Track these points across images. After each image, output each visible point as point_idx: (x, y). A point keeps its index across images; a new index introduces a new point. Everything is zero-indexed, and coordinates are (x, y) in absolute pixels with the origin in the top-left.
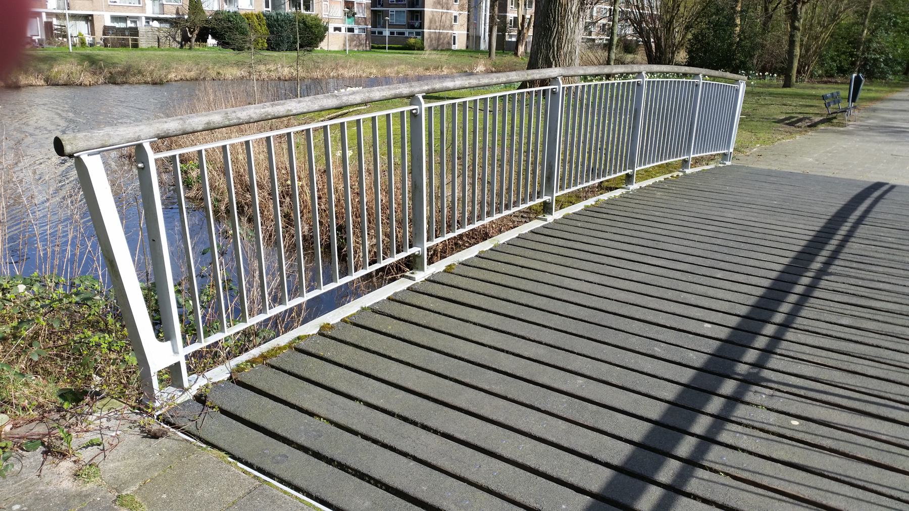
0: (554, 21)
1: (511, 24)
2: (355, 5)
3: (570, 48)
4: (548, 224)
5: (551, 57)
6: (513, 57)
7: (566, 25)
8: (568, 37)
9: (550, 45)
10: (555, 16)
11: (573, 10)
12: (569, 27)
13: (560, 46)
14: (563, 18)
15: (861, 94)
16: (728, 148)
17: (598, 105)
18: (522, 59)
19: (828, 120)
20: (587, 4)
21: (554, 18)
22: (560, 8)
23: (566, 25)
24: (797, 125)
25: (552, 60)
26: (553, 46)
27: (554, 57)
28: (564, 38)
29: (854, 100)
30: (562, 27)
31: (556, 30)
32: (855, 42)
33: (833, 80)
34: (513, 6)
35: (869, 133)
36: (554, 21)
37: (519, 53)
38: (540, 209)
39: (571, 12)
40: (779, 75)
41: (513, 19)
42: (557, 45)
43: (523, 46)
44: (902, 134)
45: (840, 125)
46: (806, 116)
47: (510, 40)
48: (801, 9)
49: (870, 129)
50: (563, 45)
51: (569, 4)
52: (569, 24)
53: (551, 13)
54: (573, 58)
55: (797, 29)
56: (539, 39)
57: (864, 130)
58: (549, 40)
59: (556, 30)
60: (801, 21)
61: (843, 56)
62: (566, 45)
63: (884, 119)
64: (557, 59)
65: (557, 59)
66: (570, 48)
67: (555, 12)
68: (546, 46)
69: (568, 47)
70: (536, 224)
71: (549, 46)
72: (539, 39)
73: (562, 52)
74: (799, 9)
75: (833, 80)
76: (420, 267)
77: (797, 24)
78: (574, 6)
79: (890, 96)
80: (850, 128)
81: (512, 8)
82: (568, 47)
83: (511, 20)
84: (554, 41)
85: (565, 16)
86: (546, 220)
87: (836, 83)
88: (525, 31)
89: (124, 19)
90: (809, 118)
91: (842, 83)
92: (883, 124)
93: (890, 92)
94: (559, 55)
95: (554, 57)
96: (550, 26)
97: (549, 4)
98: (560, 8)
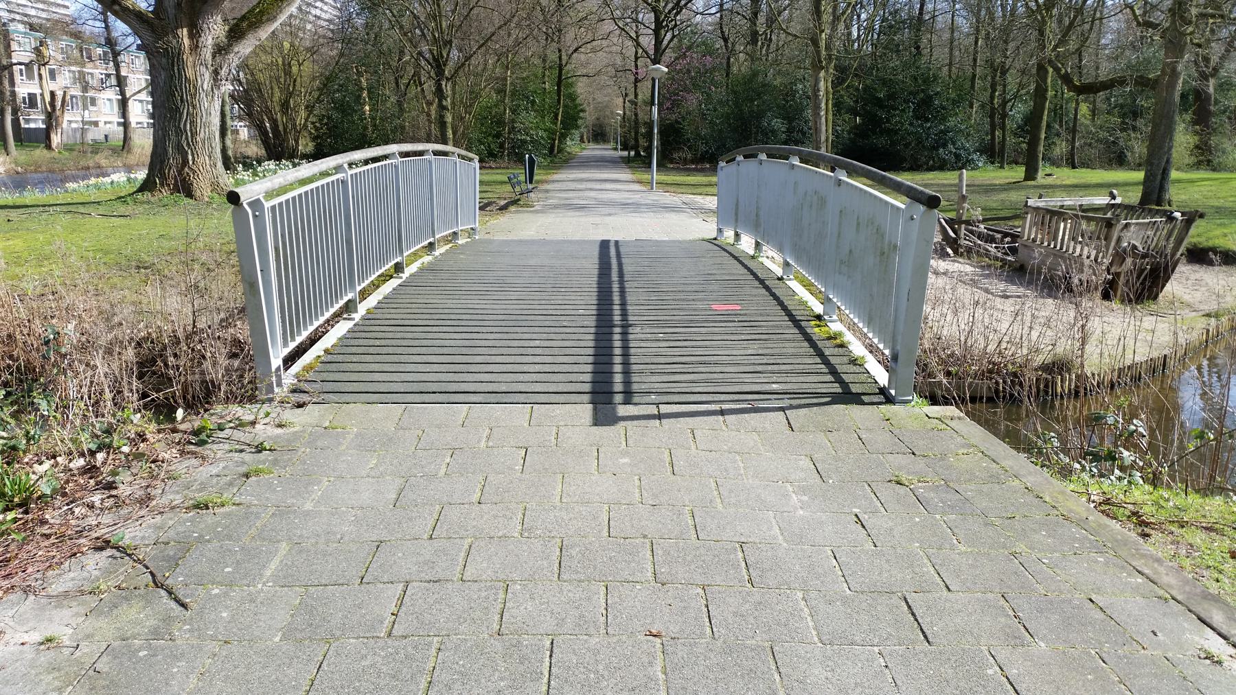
0: (182, 101)
1: (25, 103)
2: (826, 125)
3: (207, 133)
4: (404, 282)
5: (185, 145)
6: (45, 151)
7: (198, 105)
8: (204, 120)
9: (181, 130)
10: (183, 94)
11: (205, 87)
12: (202, 108)
13: (194, 131)
14: (194, 96)
15: (535, 178)
16: (475, 224)
17: (870, 171)
18: (60, 153)
19: (515, 202)
20: (221, 80)
21: (182, 97)
22: (187, 85)
23: (198, 105)
24: (488, 209)
25: (186, 148)
26: (186, 131)
27: (188, 144)
28: (199, 121)
29: (531, 182)
30: (194, 107)
31: (185, 111)
32: (500, 122)
33: (487, 165)
34: (24, 78)
35: (555, 211)
36: (182, 101)
37: (54, 145)
38: (393, 270)
39: (203, 90)
40: (981, 155)
41: (26, 96)
42: (191, 130)
43: (59, 135)
44: (586, 209)
45: (528, 206)
46: (490, 200)
47: (27, 126)
48: (446, 86)
49: (556, 207)
50: (198, 130)
51: (199, 80)
52: (202, 104)
53: (177, 90)
54: (213, 145)
55: (444, 108)
56: (164, 123)
57: (551, 208)
58: (179, 124)
59: (185, 111)
60: (449, 99)
61: (490, 139)
62: (203, 129)
63: (560, 198)
64: (193, 147)
65: (193, 147)
66: (207, 133)
67: (181, 89)
68: (176, 132)
69: (205, 132)
70: (393, 283)
71: (180, 132)
72: (164, 123)
73: (198, 139)
74: (444, 86)
75: (487, 165)
76: (353, 310)
77: (444, 103)
78: (206, 82)
79: (550, 177)
80: (537, 208)
81: (22, 80)
82: (205, 132)
83: (24, 98)
84: (185, 124)
85: (195, 95)
86: (401, 278)
87: (491, 168)
88: (58, 113)
89: (140, 123)
90: (494, 202)
91: (497, 168)
92: (562, 202)
93: (547, 174)
94: (195, 142)
95: (188, 144)
96: (177, 107)
97: (172, 78)
98: (187, 85)
